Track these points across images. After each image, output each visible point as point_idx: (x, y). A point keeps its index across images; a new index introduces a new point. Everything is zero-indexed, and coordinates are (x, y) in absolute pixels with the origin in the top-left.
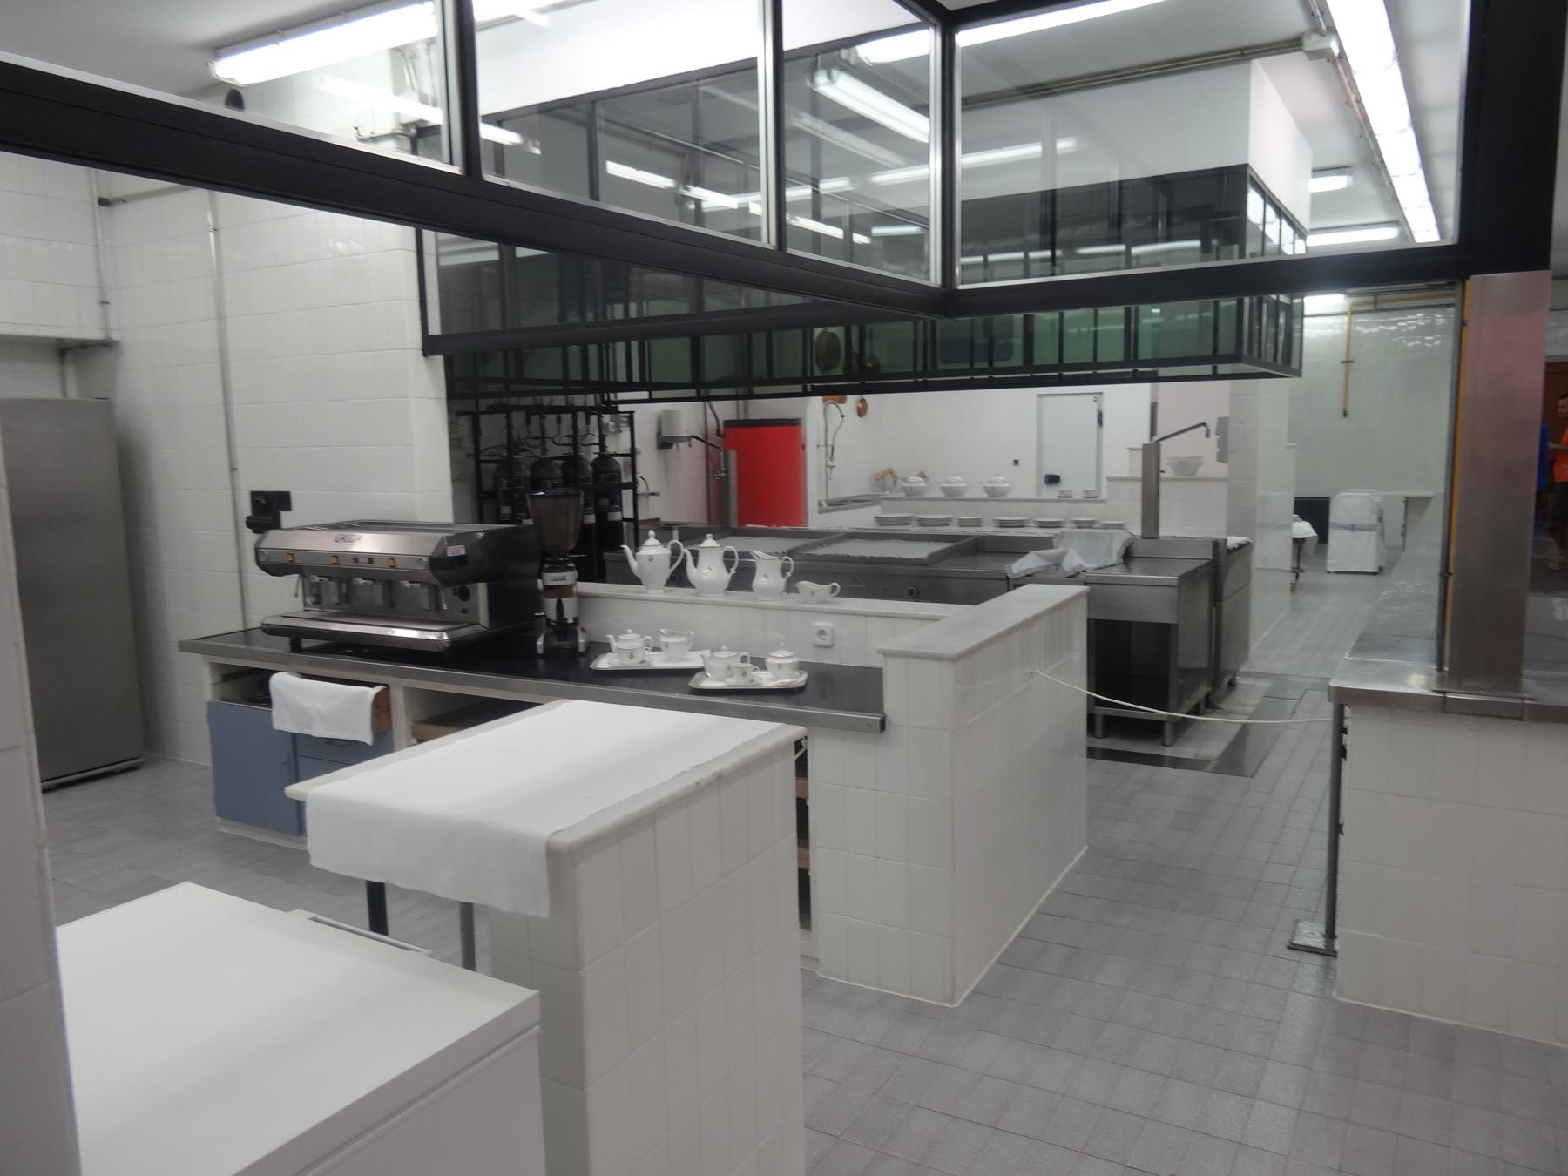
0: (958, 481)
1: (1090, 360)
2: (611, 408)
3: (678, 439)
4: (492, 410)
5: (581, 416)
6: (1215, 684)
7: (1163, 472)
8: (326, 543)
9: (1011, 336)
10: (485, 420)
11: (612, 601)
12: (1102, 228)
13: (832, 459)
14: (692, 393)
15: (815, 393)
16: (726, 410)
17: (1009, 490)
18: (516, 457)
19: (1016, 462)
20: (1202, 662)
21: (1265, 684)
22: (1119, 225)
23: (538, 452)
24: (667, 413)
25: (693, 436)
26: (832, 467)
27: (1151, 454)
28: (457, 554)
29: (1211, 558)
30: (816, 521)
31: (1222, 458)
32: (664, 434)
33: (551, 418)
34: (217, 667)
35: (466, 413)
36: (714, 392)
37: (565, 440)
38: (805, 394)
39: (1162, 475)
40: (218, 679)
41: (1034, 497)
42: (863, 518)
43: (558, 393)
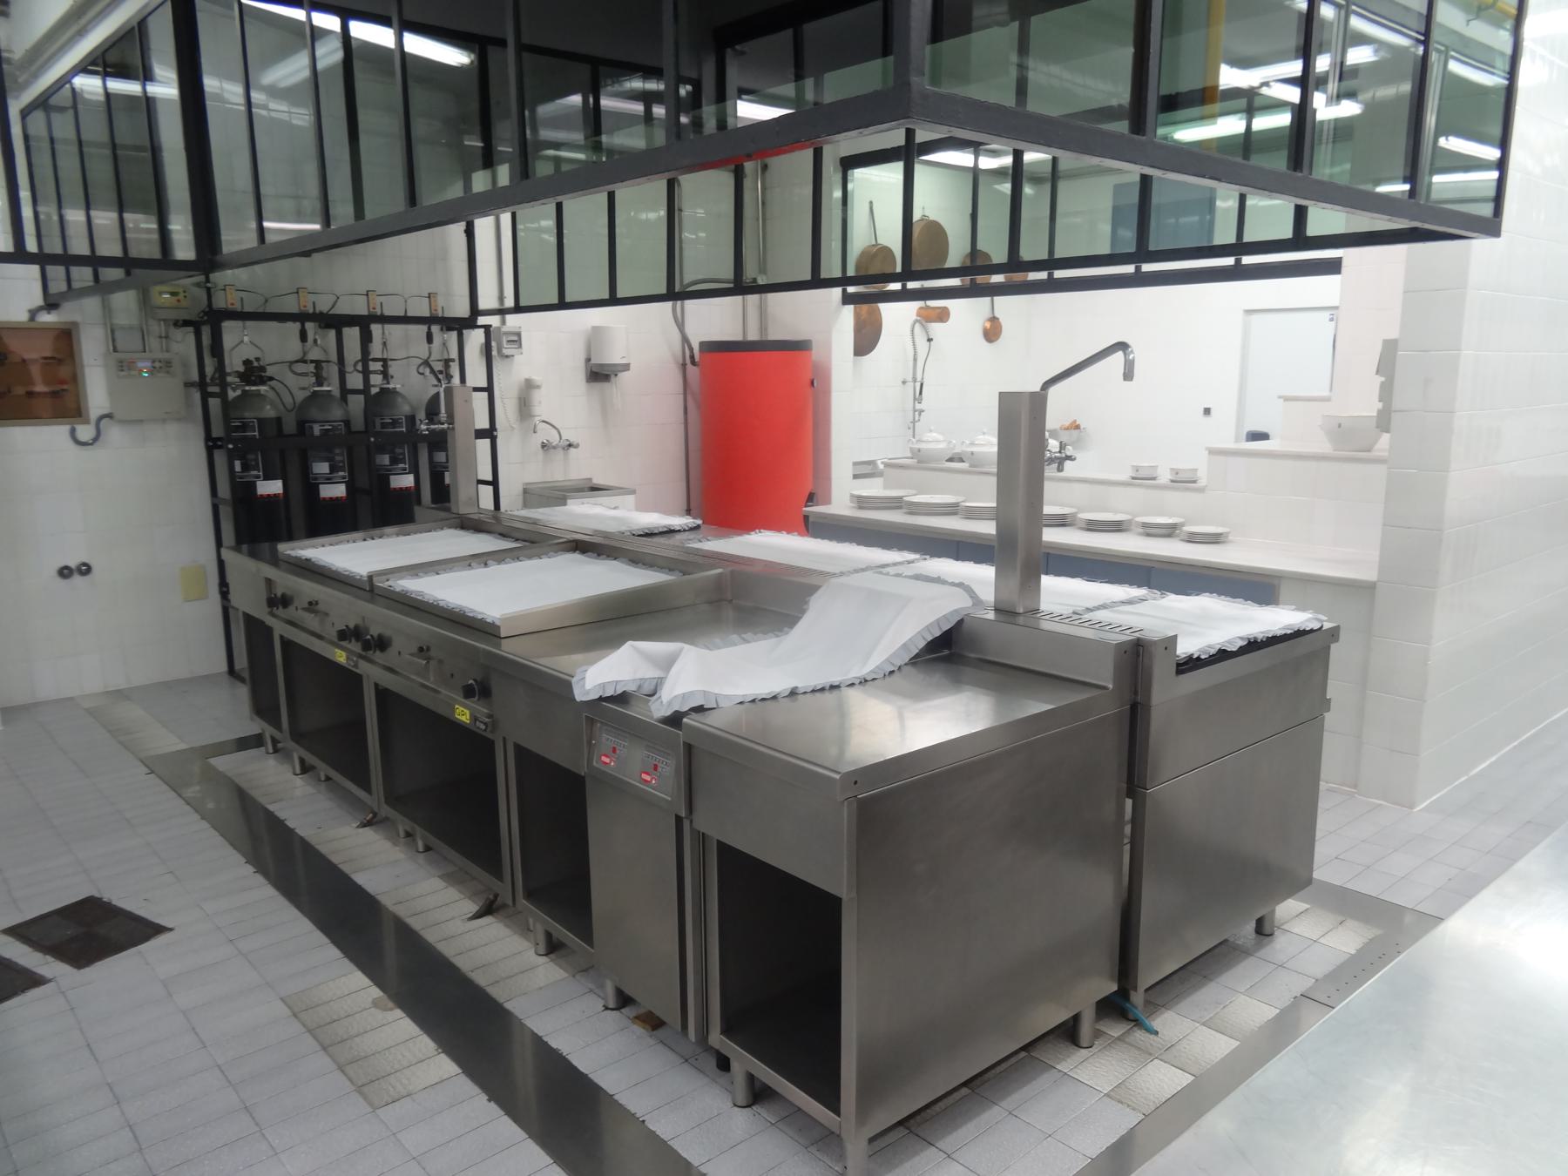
19: (1207, 411)
26: (921, 411)
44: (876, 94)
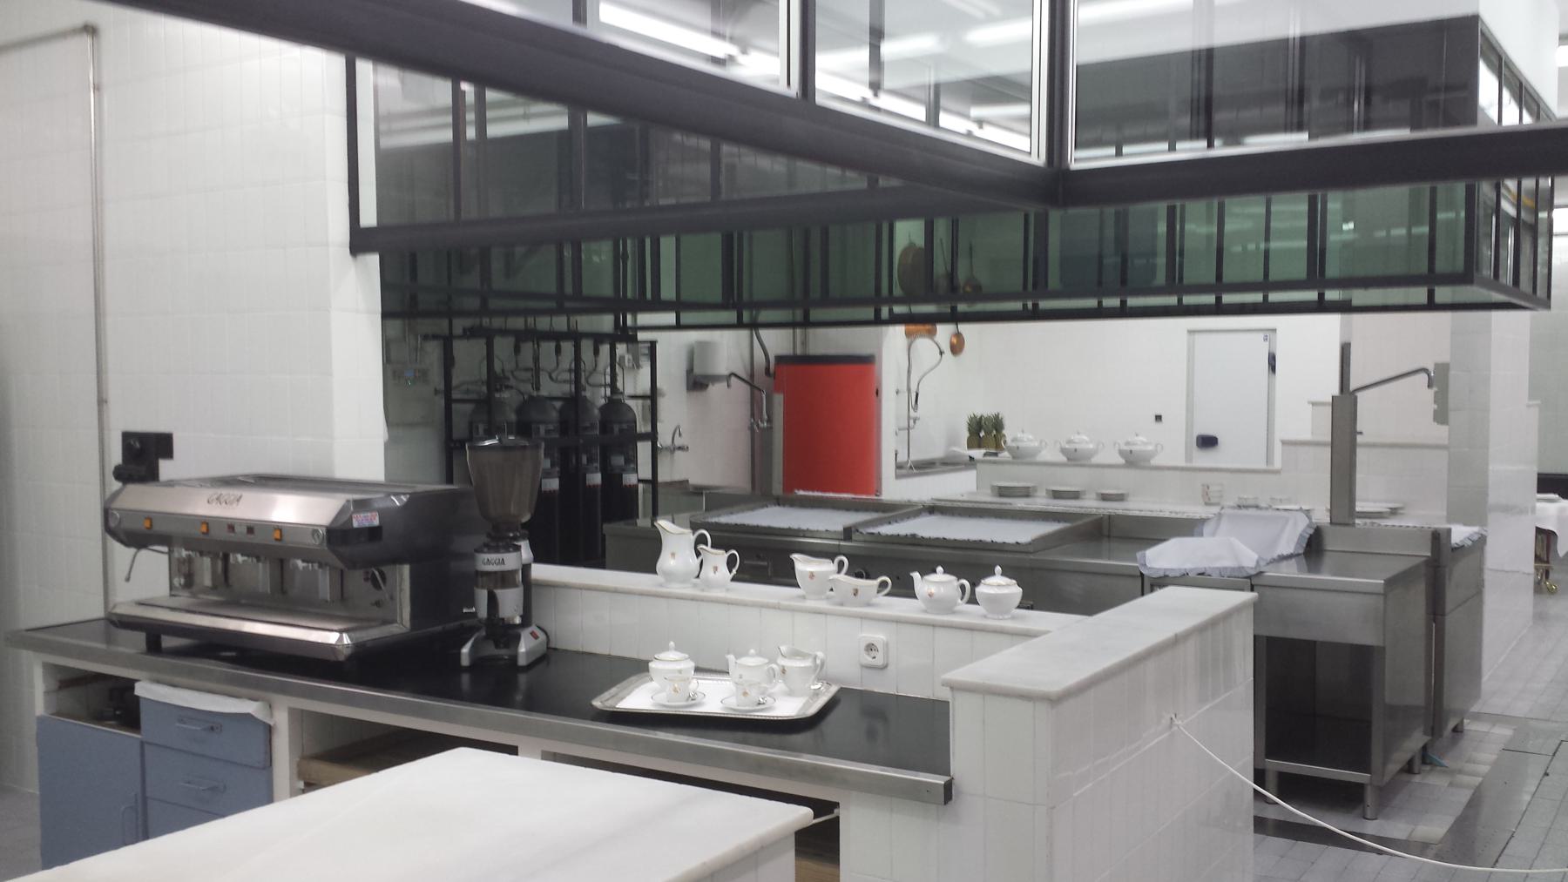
0: (1084, 442)
1: (1260, 277)
2: (626, 335)
3: (716, 379)
4: (470, 333)
5: (587, 346)
6: (1435, 730)
7: (1361, 433)
8: (203, 505)
9: (1154, 254)
10: (460, 347)
11: (594, 594)
12: (1278, 111)
13: (915, 409)
14: (730, 316)
15: (895, 320)
16: (777, 341)
17: (1036, 451)
18: (497, 395)
19: (1159, 418)
20: (1416, 696)
21: (1503, 732)
22: (1301, 103)
23: (528, 388)
24: (703, 346)
25: (733, 374)
27: (1345, 406)
28: (367, 524)
29: (1429, 554)
30: (893, 489)
31: (1441, 416)
32: (697, 371)
33: (548, 347)
34: (50, 669)
35: (435, 337)
36: (765, 316)
37: (566, 376)
38: (878, 321)
39: (1359, 439)
40: (54, 685)
41: (1182, 463)
42: (958, 486)
43: (550, 312)
44: (581, 292)
